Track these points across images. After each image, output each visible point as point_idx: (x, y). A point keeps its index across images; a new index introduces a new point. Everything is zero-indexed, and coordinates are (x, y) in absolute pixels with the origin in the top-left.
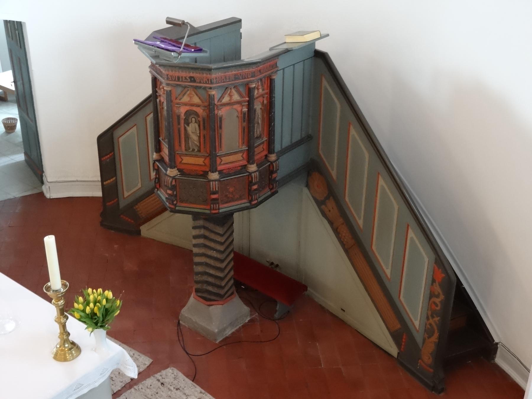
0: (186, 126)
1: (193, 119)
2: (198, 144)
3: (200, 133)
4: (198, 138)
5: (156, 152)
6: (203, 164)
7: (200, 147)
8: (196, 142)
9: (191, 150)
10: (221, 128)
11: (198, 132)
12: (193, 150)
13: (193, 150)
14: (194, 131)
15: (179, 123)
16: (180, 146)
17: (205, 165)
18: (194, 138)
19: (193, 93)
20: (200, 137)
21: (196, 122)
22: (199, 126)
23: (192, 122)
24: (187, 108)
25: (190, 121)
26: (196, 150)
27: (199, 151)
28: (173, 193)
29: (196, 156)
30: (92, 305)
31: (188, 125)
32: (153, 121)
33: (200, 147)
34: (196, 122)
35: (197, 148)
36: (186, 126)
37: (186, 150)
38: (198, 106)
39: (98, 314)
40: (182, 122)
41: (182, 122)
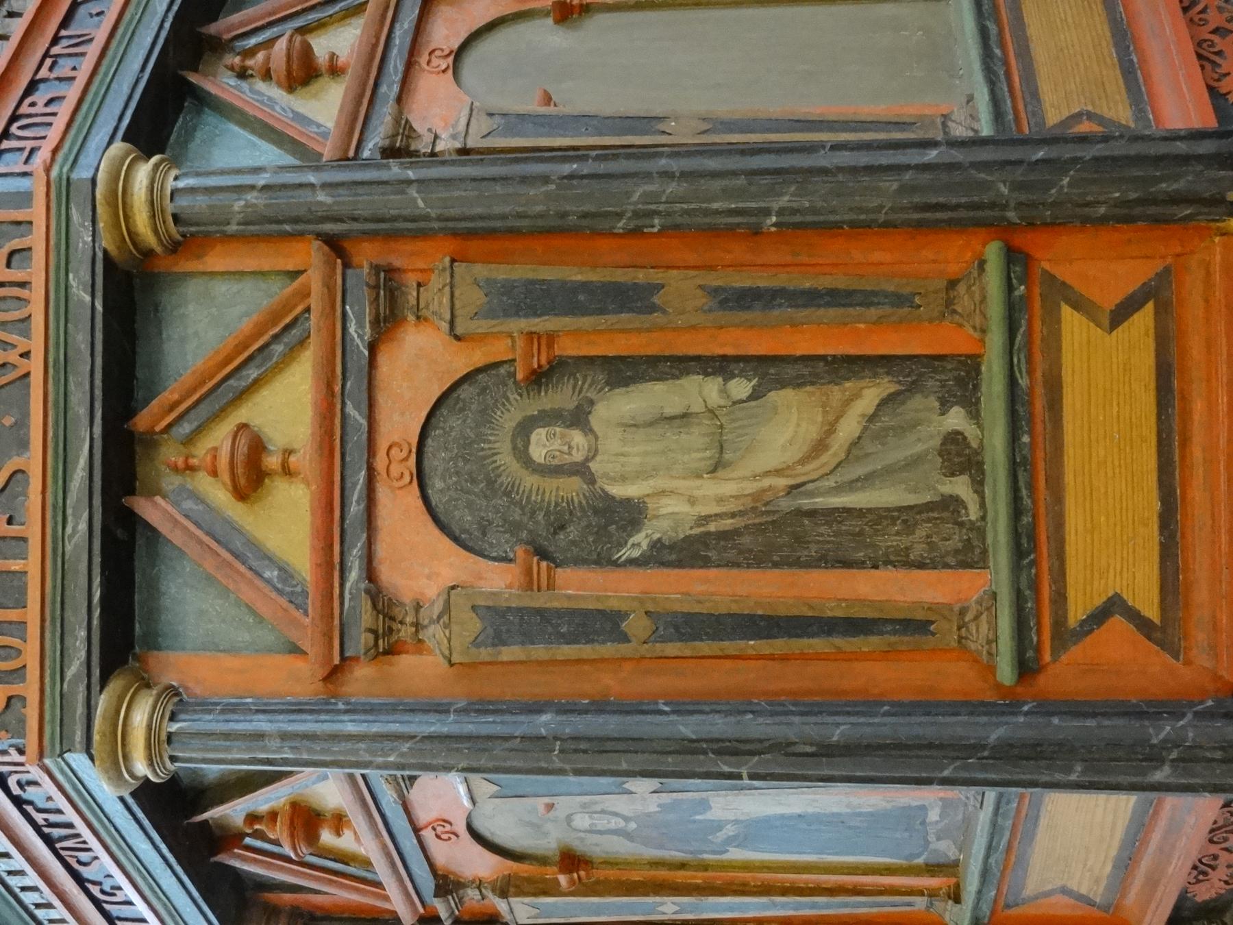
0: (641, 541)
1: (541, 445)
2: (871, 394)
3: (721, 366)
4: (781, 397)
5: (593, 703)
6: (1144, 319)
7: (910, 370)
8: (849, 428)
9: (960, 486)
10: (647, 122)
11: (704, 391)
12: (959, 456)
13: (959, 456)
14: (696, 438)
15: (601, 624)
16: (914, 626)
17: (1156, 293)
18: (783, 438)
19: (220, 437)
20: (772, 371)
21: (578, 418)
22: (624, 371)
23: (581, 470)
24: (399, 509)
25: (572, 487)
26: (956, 419)
27: (962, 381)
28: (1026, 432)
29: (1033, 412)
30: (758, 504)
31: (630, 515)
32: (315, 806)
33: (910, 370)
34: (578, 418)
35: (923, 404)
36: (641, 541)
37: (971, 556)
38: (350, 389)
39: (275, 92)
40: (578, 586)
41: (578, 586)
